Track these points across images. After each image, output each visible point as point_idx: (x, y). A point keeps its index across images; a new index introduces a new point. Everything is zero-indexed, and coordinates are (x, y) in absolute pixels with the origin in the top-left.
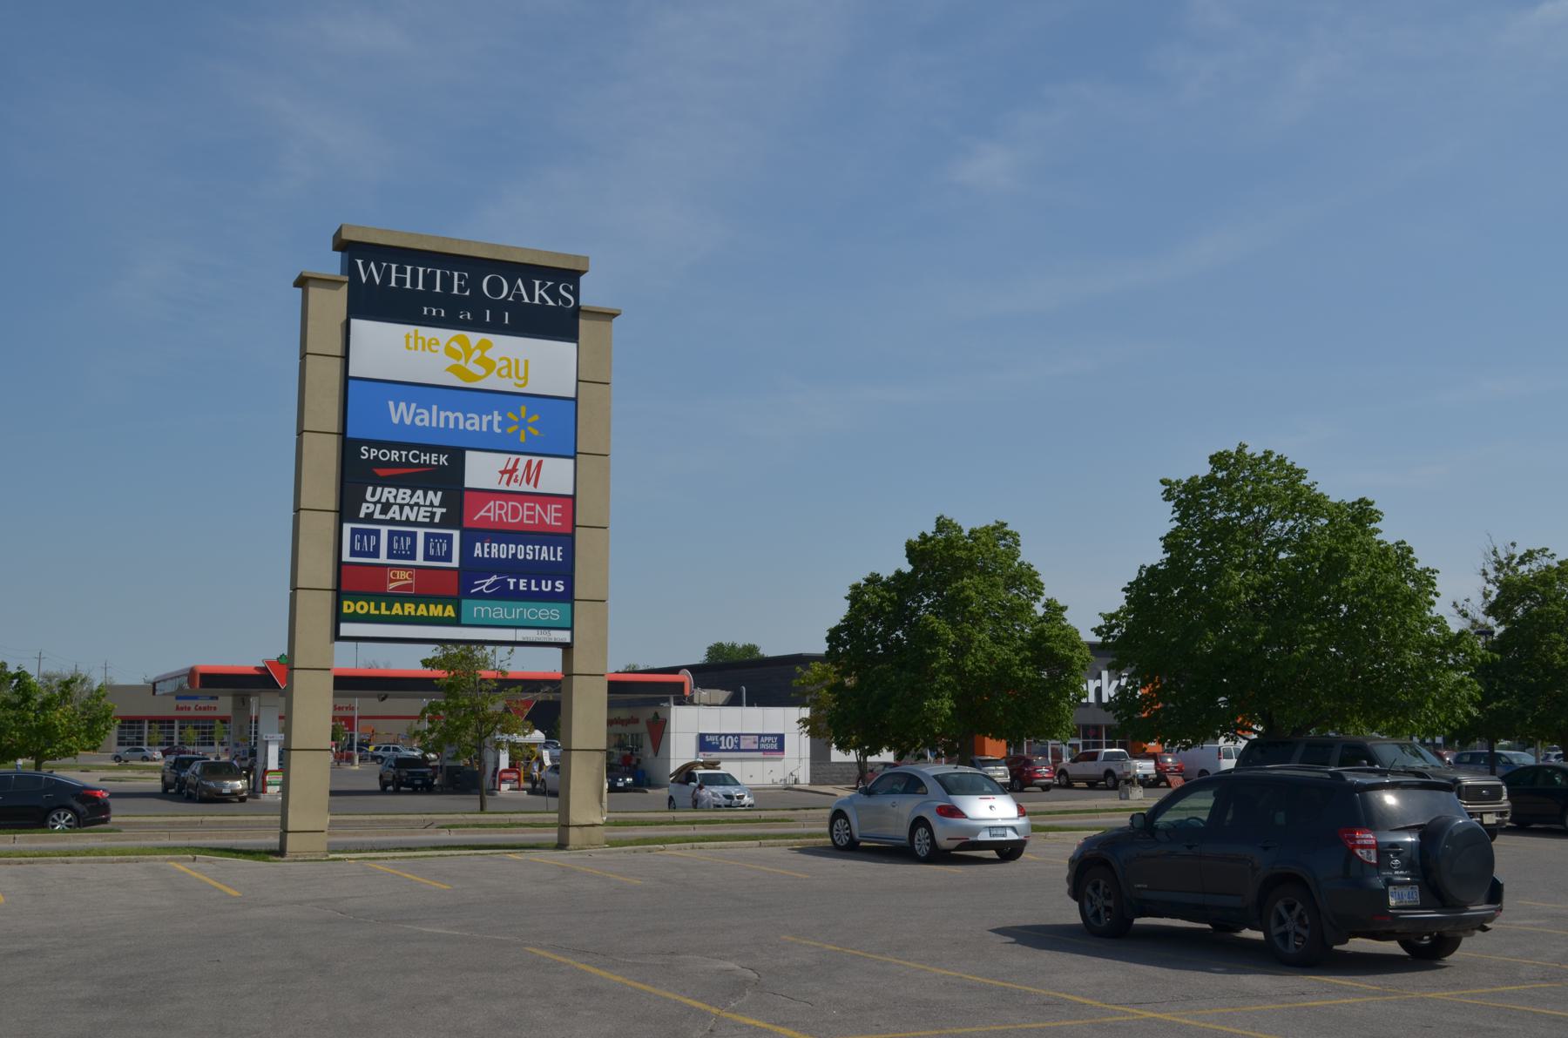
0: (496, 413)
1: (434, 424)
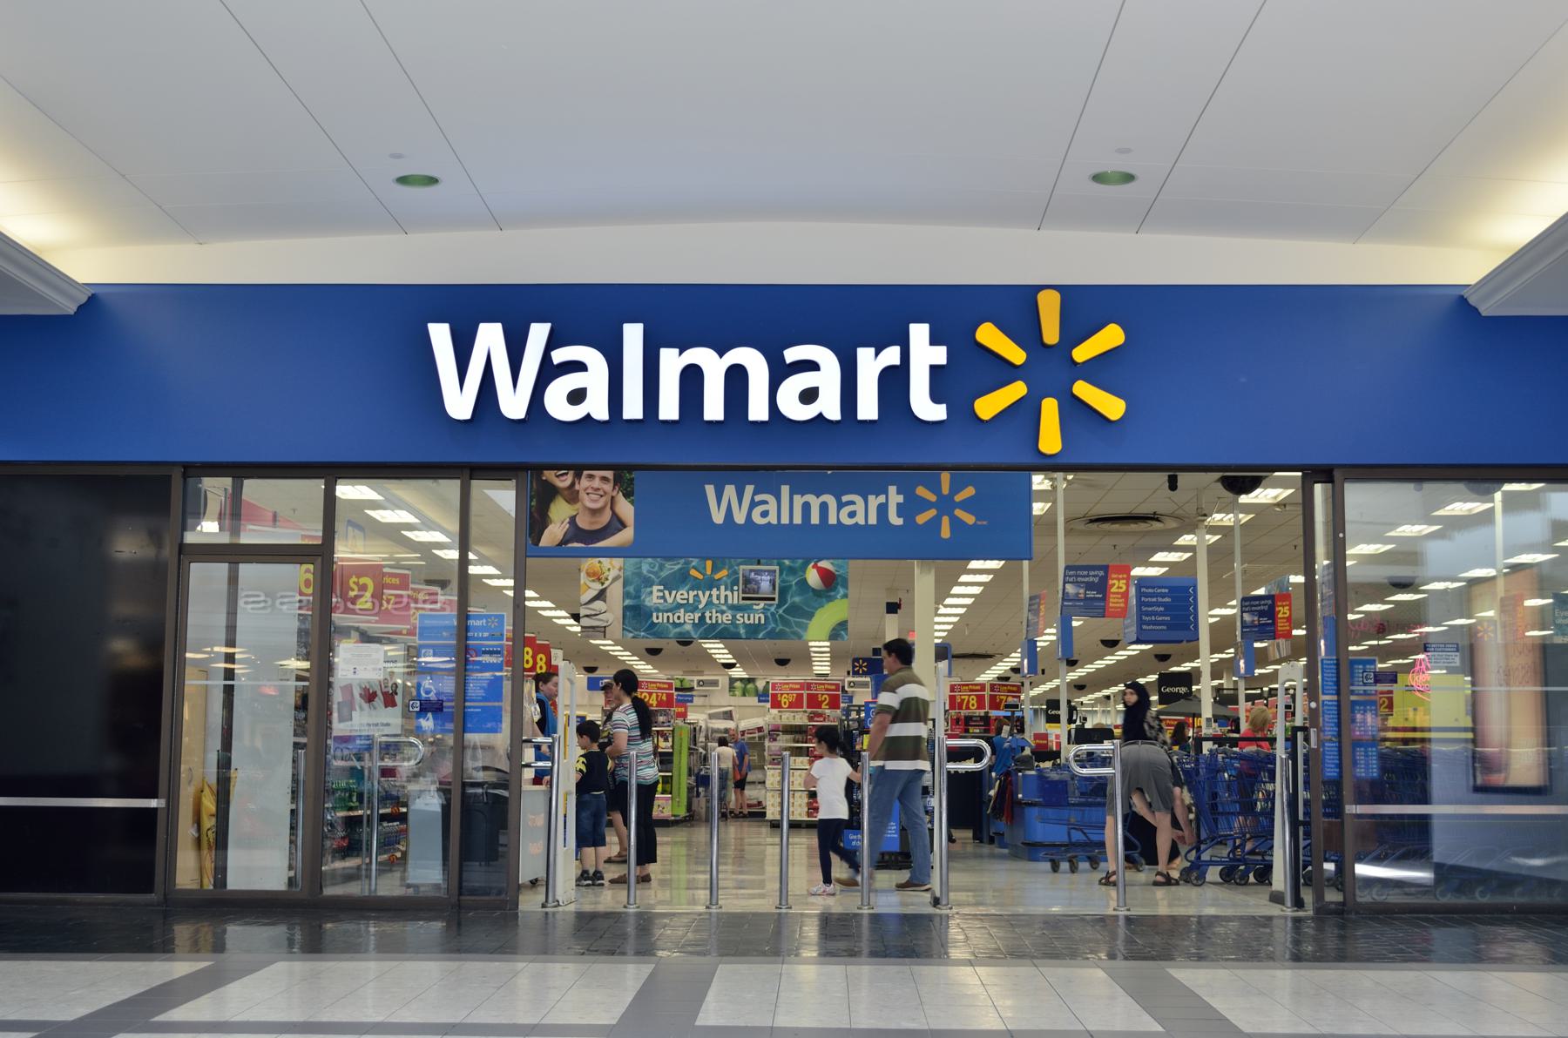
0: (919, 333)
1: (633, 408)
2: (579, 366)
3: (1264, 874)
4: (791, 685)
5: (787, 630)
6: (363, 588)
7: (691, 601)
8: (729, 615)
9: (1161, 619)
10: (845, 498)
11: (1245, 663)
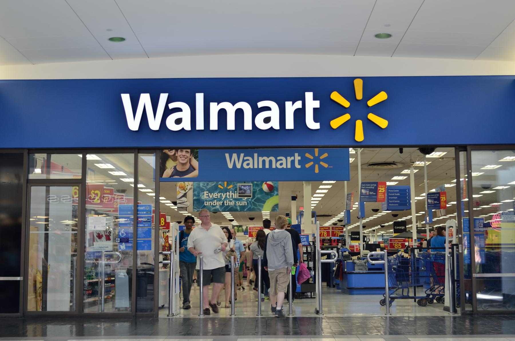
0: (309, 96)
1: (200, 125)
2: (179, 110)
3: (441, 299)
4: (256, 228)
5: (255, 207)
6: (97, 194)
7: (219, 197)
8: (233, 202)
9: (396, 201)
10: (278, 158)
11: (429, 218)
